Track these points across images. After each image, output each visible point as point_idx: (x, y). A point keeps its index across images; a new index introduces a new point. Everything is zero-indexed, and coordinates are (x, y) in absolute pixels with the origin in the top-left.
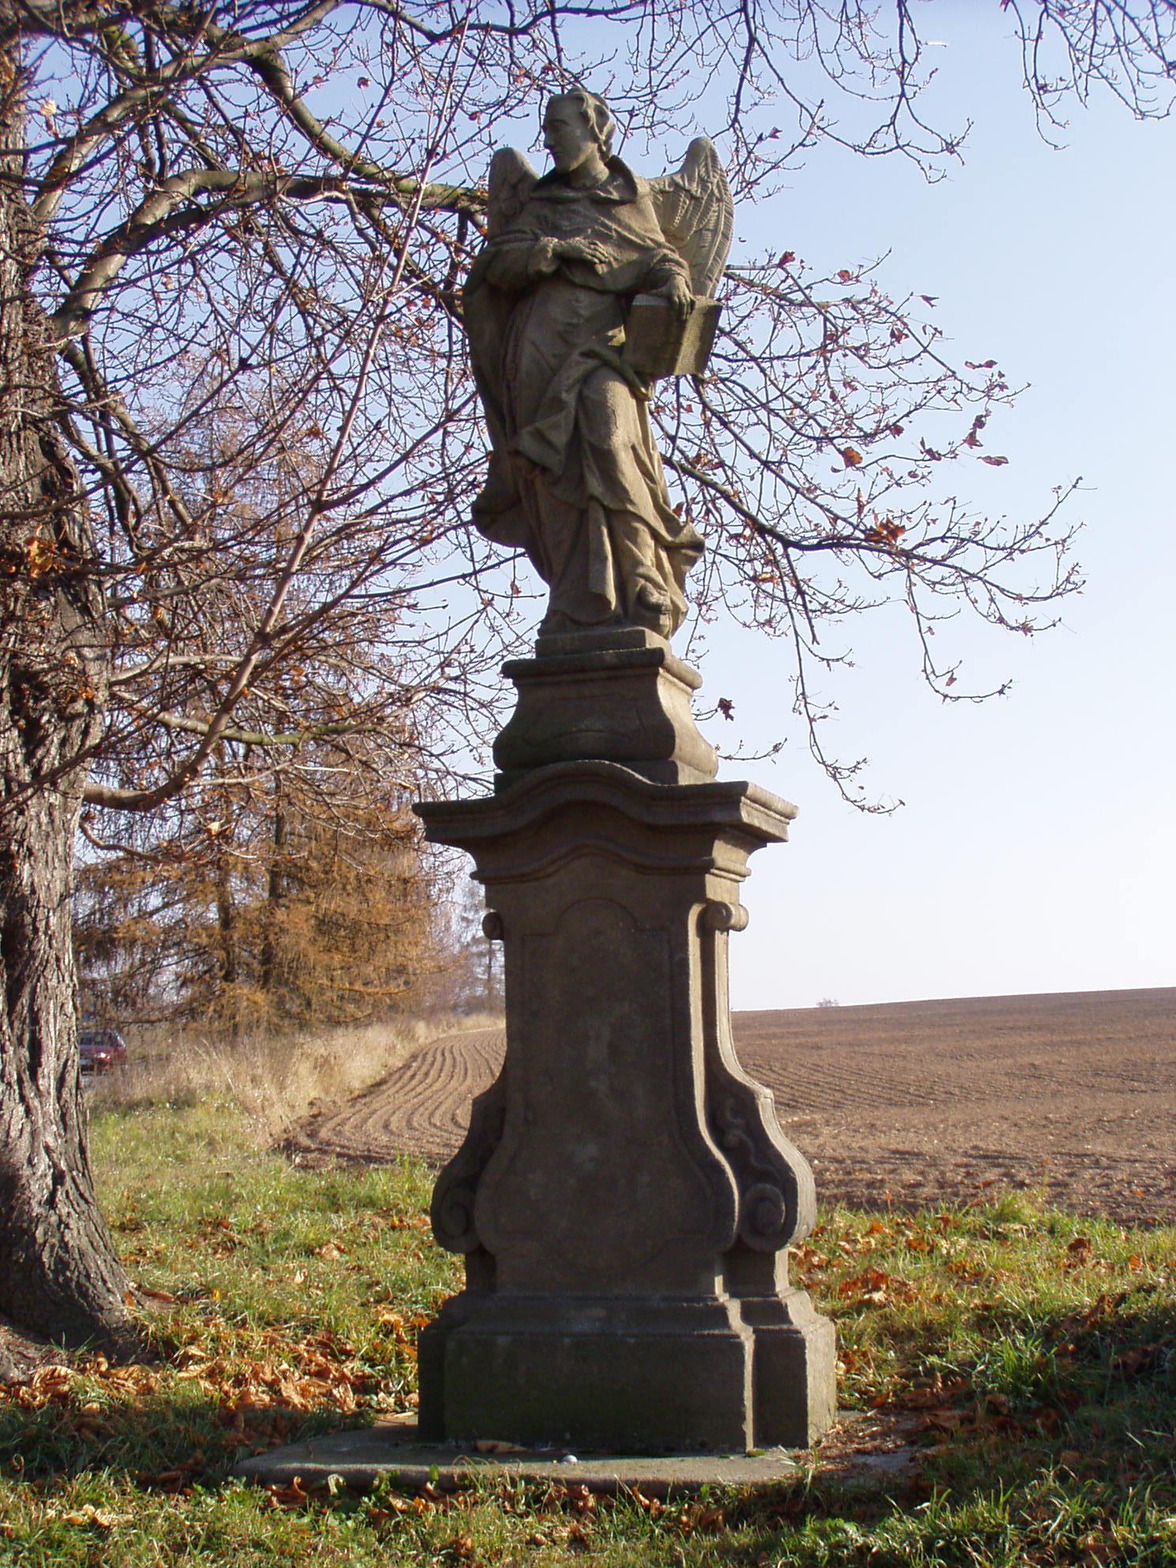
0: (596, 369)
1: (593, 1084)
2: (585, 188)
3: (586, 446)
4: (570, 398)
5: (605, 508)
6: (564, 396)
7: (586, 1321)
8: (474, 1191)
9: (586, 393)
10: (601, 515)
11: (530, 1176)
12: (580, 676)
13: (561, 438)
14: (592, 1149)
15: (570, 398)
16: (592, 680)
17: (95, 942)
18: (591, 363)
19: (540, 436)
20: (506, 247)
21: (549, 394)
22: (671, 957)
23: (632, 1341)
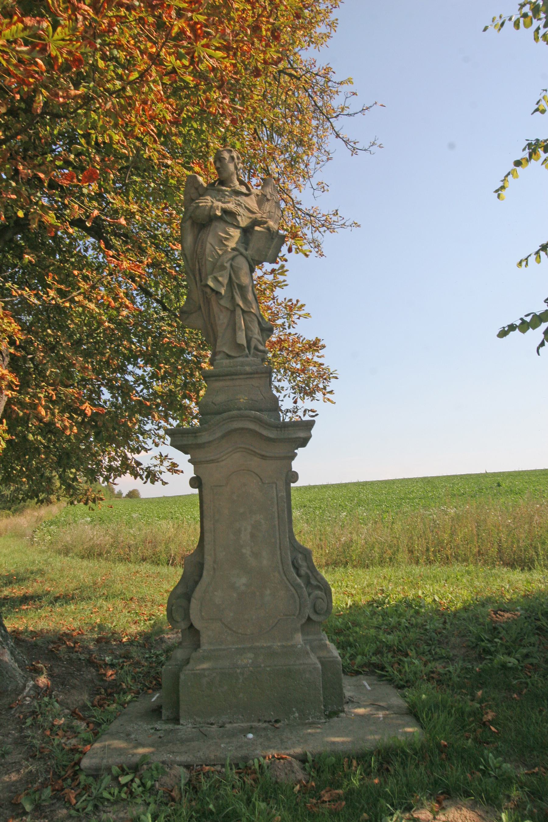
0: (236, 256)
1: (244, 551)
2: (230, 187)
3: (235, 284)
4: (228, 265)
5: (242, 309)
6: (225, 264)
7: (247, 660)
8: (189, 601)
9: (233, 264)
10: (241, 312)
11: (215, 593)
12: (217, 378)
13: (224, 280)
14: (244, 580)
15: (228, 265)
16: (240, 379)
17: (442, 776)
18: (236, 253)
19: (216, 279)
20: (201, 205)
21: (218, 264)
22: (277, 495)
23: (268, 669)
